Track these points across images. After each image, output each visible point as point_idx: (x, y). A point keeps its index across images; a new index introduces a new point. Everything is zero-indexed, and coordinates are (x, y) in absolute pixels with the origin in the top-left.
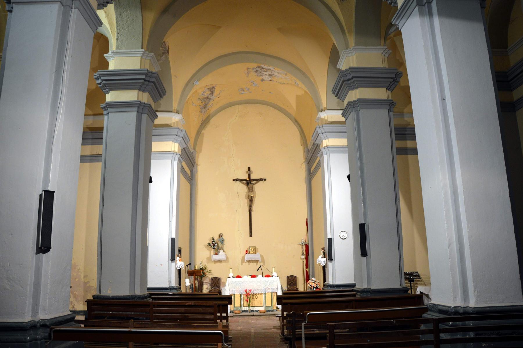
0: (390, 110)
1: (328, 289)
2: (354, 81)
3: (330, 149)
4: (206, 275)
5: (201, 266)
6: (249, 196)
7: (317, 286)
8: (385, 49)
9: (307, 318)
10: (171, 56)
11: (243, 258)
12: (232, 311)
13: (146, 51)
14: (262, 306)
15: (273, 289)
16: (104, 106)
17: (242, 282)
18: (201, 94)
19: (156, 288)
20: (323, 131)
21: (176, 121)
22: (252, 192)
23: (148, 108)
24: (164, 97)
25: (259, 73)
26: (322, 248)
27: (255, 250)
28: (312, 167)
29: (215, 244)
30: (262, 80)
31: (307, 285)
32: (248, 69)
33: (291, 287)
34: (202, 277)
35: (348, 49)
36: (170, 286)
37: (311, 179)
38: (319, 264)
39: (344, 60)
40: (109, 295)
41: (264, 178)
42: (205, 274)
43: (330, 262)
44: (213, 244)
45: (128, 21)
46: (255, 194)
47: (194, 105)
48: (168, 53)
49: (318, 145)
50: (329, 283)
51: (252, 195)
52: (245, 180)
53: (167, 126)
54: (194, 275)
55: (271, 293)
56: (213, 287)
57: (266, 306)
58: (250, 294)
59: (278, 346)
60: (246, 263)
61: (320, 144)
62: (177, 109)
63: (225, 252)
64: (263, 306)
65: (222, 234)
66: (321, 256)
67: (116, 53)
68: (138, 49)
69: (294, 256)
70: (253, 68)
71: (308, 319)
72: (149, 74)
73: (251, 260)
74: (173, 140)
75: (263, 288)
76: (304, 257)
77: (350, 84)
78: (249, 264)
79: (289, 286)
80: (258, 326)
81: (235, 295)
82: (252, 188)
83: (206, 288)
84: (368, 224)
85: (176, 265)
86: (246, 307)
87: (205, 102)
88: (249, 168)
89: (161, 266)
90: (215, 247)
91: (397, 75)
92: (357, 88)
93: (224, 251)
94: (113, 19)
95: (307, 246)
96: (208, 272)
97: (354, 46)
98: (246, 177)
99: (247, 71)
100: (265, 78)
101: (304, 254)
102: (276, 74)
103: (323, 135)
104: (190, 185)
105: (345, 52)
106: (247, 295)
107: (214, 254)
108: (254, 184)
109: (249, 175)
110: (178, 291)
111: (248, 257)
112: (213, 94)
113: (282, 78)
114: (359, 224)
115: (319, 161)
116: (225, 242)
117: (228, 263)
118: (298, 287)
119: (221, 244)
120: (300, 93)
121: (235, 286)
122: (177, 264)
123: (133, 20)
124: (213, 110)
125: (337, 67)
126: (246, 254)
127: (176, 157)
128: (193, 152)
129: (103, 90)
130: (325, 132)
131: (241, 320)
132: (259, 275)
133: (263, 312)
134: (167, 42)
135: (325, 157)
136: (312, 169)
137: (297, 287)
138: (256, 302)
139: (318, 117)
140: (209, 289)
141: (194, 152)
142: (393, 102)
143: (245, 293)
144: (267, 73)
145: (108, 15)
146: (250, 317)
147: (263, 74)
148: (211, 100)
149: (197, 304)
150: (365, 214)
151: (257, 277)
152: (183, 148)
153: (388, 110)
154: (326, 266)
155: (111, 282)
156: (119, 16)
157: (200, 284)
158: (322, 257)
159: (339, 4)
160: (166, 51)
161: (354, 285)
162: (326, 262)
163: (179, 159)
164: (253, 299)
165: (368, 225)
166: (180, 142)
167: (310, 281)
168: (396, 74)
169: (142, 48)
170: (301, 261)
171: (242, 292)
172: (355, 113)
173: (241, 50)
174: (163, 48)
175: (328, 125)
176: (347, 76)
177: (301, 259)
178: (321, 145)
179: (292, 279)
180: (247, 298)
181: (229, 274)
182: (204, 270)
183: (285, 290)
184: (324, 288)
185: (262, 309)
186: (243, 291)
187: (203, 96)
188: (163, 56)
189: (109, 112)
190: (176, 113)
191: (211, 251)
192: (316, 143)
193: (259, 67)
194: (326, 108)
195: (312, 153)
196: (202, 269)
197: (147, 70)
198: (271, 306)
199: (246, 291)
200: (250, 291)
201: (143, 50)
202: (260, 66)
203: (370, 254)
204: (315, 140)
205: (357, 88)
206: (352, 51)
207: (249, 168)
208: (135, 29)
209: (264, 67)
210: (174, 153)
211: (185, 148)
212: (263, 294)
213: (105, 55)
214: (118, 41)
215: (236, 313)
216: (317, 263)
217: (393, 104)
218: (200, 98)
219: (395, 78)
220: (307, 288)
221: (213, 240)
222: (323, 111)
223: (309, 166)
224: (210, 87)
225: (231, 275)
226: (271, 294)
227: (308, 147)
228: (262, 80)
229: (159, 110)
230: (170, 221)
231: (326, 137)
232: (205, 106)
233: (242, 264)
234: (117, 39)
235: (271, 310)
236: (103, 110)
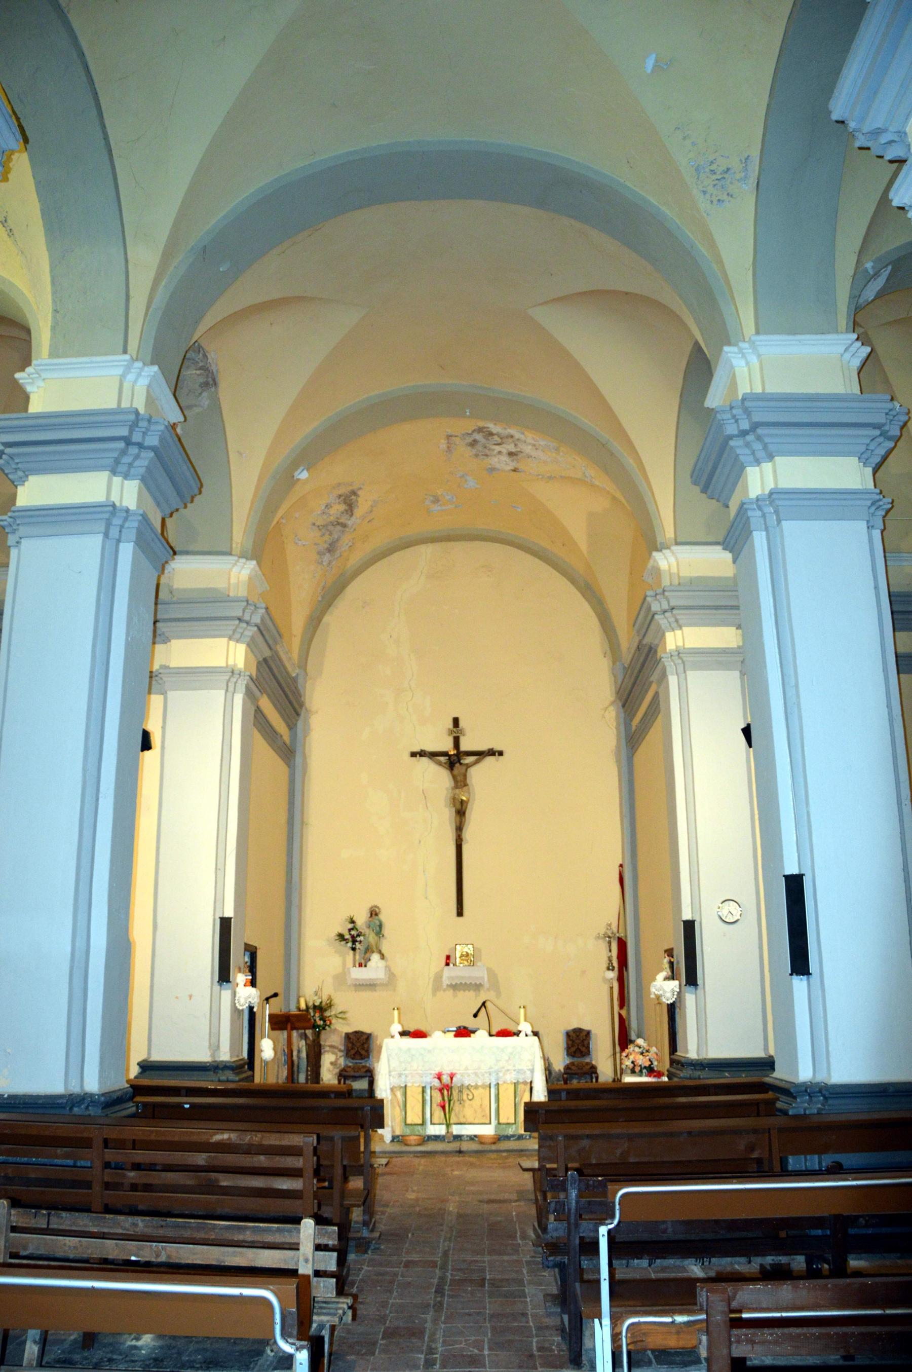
1: (685, 1073)
4: (332, 1027)
5: (316, 998)
6: (454, 799)
7: (652, 1064)
9: (617, 1207)
11: (438, 977)
12: (398, 1136)
13: (133, 360)
14: (488, 1122)
15: (519, 1071)
16: (9, 520)
17: (430, 1051)
20: (665, 606)
25: (480, 449)
29: (358, 935)
31: (621, 1060)
34: (318, 1030)
36: (217, 1059)
38: (658, 997)
42: (328, 1023)
44: (353, 937)
47: (300, 543)
51: (464, 798)
54: (289, 1027)
55: (515, 1083)
60: (444, 990)
61: (657, 645)
64: (490, 1123)
65: (378, 908)
66: (662, 975)
70: (463, 435)
71: (621, 1210)
73: (466, 983)
75: (490, 1068)
76: (612, 975)
78: (455, 996)
82: (465, 776)
83: (332, 1063)
85: (235, 997)
87: (330, 534)
88: (456, 721)
90: (358, 945)
93: (383, 957)
95: (622, 945)
98: (447, 745)
100: (499, 462)
102: (528, 449)
103: (666, 618)
104: (289, 767)
106: (441, 1090)
107: (354, 966)
108: (468, 766)
112: (352, 511)
115: (656, 695)
116: (386, 931)
117: (394, 990)
119: (376, 938)
122: (238, 995)
127: (239, 682)
128: (297, 675)
131: (421, 1168)
135: (673, 680)
138: (468, 1111)
143: (436, 1083)
144: (505, 449)
148: (347, 530)
151: (472, 1035)
152: (261, 659)
153: (865, 522)
154: (677, 1004)
155: (9, 1050)
158: (667, 979)
161: (768, 1064)
162: (679, 993)
163: (248, 688)
164: (461, 1101)
166: (252, 638)
167: (632, 1049)
168: (887, 414)
170: (605, 989)
174: (201, 368)
177: (605, 980)
178: (659, 650)
179: (579, 1039)
182: (326, 1010)
183: (560, 1070)
185: (488, 1131)
186: (432, 1076)
187: (325, 517)
195: (635, 675)
196: (319, 1009)
198: (513, 1121)
199: (439, 1078)
200: (452, 1078)
201: (127, 357)
202: (484, 428)
207: (456, 721)
213: (18, 375)
216: (652, 996)
218: (318, 523)
220: (622, 1070)
221: (351, 926)
223: (625, 712)
224: (343, 490)
225: (396, 1028)
226: (513, 1086)
228: (492, 470)
230: (219, 870)
232: (330, 545)
233: (434, 994)
235: (513, 1136)
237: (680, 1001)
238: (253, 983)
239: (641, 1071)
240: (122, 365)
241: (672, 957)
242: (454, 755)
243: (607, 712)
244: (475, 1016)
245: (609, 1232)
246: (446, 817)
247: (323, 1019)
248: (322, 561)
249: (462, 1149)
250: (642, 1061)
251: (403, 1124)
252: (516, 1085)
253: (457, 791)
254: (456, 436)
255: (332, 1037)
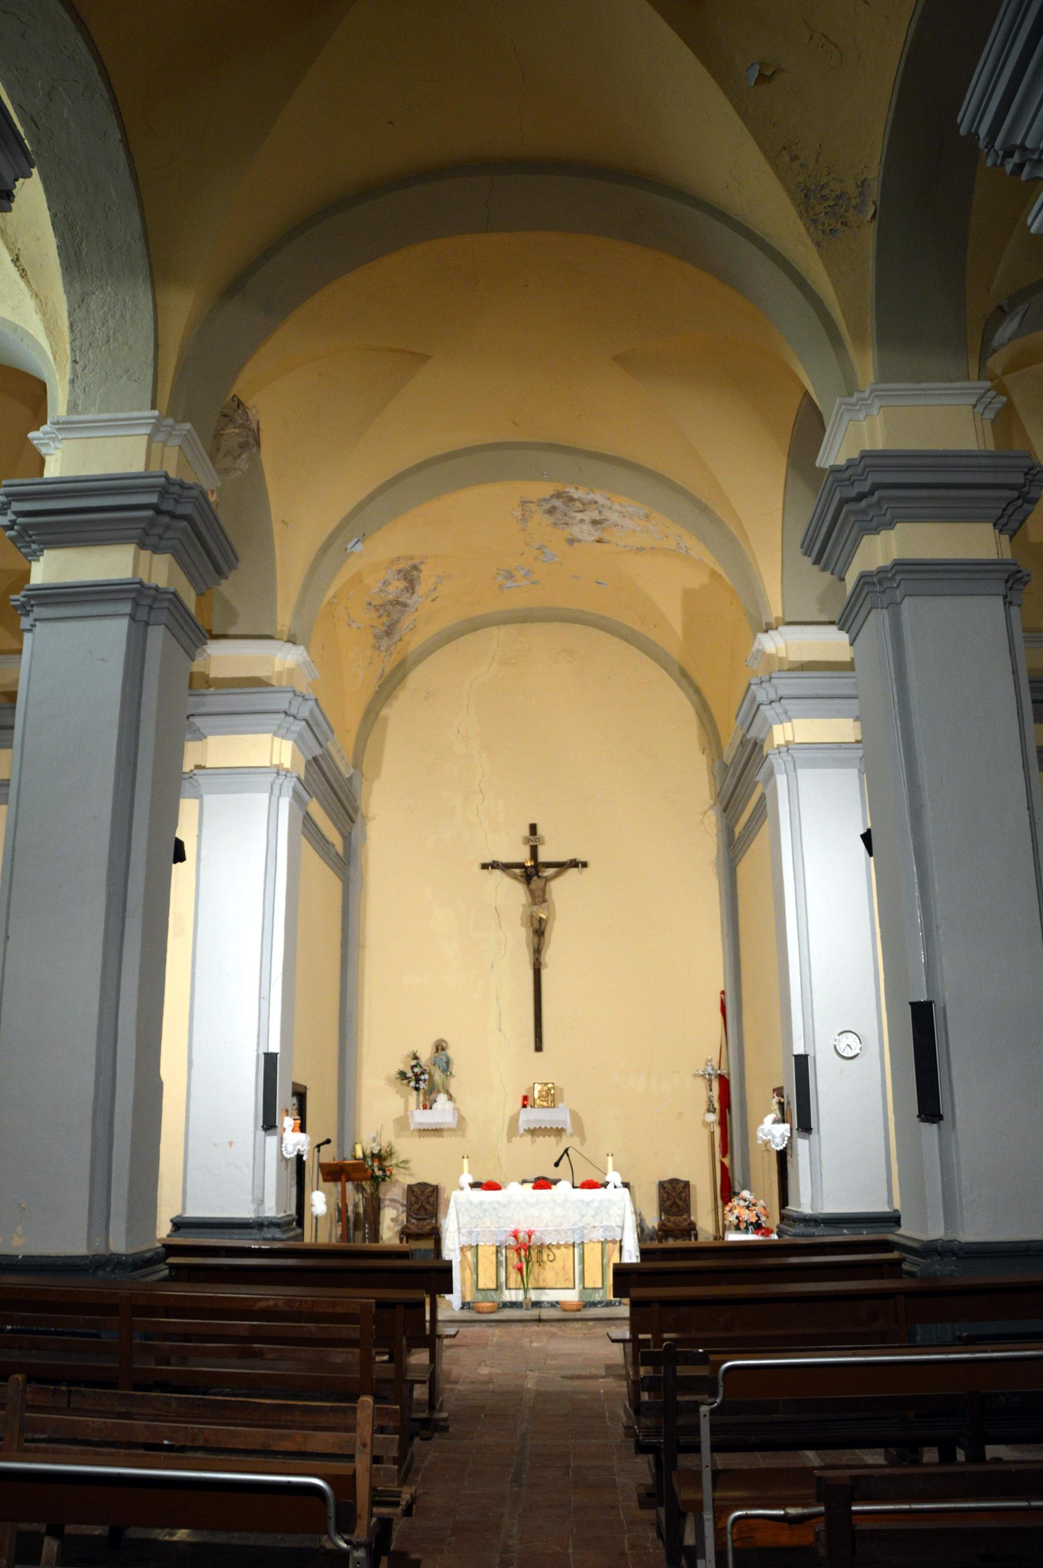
0: (1008, 599)
2: (881, 499)
3: (797, 754)
4: (393, 1178)
5: (374, 1145)
6: (532, 916)
7: (759, 1219)
8: (983, 391)
9: (721, 1383)
10: (267, 456)
11: (514, 1120)
12: (469, 1303)
14: (572, 1286)
15: (607, 1228)
16: (22, 599)
17: (504, 1206)
18: (376, 590)
19: (211, 1221)
21: (288, 669)
22: (543, 905)
23: (166, 604)
24: (232, 575)
25: (560, 517)
26: (774, 1090)
27: (551, 1097)
28: (737, 821)
29: (422, 1073)
30: (572, 541)
31: (724, 1215)
32: (524, 503)
33: (672, 1219)
34: (376, 1181)
35: (856, 395)
36: (261, 1215)
37: (737, 861)
38: (767, 1143)
39: (838, 441)
40: (16, 1254)
41: (583, 859)
42: (388, 1173)
43: (804, 1138)
44: (416, 1075)
45: (107, 321)
46: (551, 912)
48: (258, 444)
49: (756, 744)
50: (799, 1210)
51: (544, 916)
52: (520, 866)
53: (256, 683)
55: (602, 1242)
56: (415, 1216)
57: (584, 1288)
58: (529, 1247)
59: (615, 1457)
60: (521, 1136)
61: (763, 740)
62: (289, 630)
63: (455, 1102)
64: (574, 1288)
66: (771, 1117)
67: (65, 426)
68: (140, 409)
69: (681, 1114)
71: (725, 1386)
72: (172, 489)
73: (540, 1128)
74: (275, 728)
76: (713, 1118)
77: (864, 512)
78: (533, 1142)
79: (665, 1213)
80: (553, 1362)
81: (480, 1248)
82: (544, 890)
83: (392, 1220)
84: (942, 1005)
86: (516, 1289)
87: (389, 615)
88: (533, 828)
89: (231, 1146)
90: (422, 1085)
91: (1030, 477)
92: (890, 525)
93: (450, 1098)
94: (61, 317)
95: (724, 1082)
96: (397, 1166)
97: (876, 383)
98: (523, 856)
99: (521, 508)
100: (582, 532)
101: (715, 1109)
102: (614, 517)
103: (773, 709)
105: (843, 407)
106: (518, 1251)
107: (418, 1108)
108: (547, 880)
109: (534, 852)
110: (284, 1232)
111: (530, 1117)
113: (634, 531)
114: (911, 1004)
115: (763, 797)
116: (455, 1069)
117: (464, 1136)
118: (696, 1216)
119: (443, 1076)
120: (697, 579)
121: (480, 1218)
123: (123, 317)
124: (415, 642)
125: (817, 464)
126: (524, 1106)
127: (286, 784)
129: (22, 550)
130: (781, 698)
131: (495, 1339)
132: (565, 1180)
133: (575, 1308)
134: (255, 407)
135: (781, 780)
136: (738, 829)
137: (692, 1218)
138: (549, 1273)
139: (754, 649)
140: (402, 1221)
141: (354, 778)
142: (1019, 572)
143: (512, 1241)
145: (44, 304)
146: (530, 1324)
147: (574, 518)
148: (408, 610)
149: (297, 1305)
150: (930, 967)
151: (553, 1187)
152: (310, 758)
154: (789, 1151)
155: (23, 1205)
156: (79, 307)
157: (373, 1207)
158: (775, 1122)
159: (818, 245)
160: (252, 441)
161: (893, 1220)
162: (790, 1138)
164: (540, 1262)
165: (944, 1009)
166: (300, 734)
168: (1026, 474)
169: (153, 407)
170: (706, 1132)
171: (503, 1238)
172: (885, 611)
173: (498, 439)
175: (787, 674)
176: (854, 481)
177: (707, 1125)
179: (676, 1192)
180: (521, 1261)
181: (459, 1177)
182: (385, 1159)
183: (653, 1227)
184: (784, 1227)
185: (571, 1296)
186: (507, 1234)
187: (383, 596)
188: (240, 454)
189: (36, 620)
190: (288, 641)
191: (410, 1097)
192: (749, 736)
193: (559, 495)
194: (783, 618)
197: (166, 476)
198: (600, 1286)
200: (530, 1237)
201: (156, 413)
203: (953, 1114)
204: (746, 726)
205: (890, 525)
206: (869, 402)
207: (533, 828)
208: (130, 347)
209: (576, 494)
210: (278, 773)
211: (320, 759)
212: (574, 1247)
213: (31, 435)
214: (73, 387)
215: (481, 1310)
216: (760, 1142)
217: (1022, 578)
218: (374, 603)
219: (1024, 486)
220: (724, 1226)
221: (414, 1062)
222: (772, 629)
223: (727, 818)
224: (404, 565)
225: (466, 1179)
226: (600, 1245)
227: (725, 758)
228: (572, 541)
229: (231, 631)
230: (263, 998)
231: (784, 716)
232: (389, 627)
233: (509, 1140)
234: (72, 382)
235: (600, 1302)
236: (21, 615)
237: (791, 1148)
238: (303, 1128)
239: (747, 1228)
240: (152, 423)
241: (783, 1097)
242: (531, 866)
243: (706, 816)
244: (557, 1165)
245: (712, 1412)
246: (520, 937)
247: (382, 1168)
248: (380, 646)
249: (542, 1318)
250: (748, 1216)
251: (474, 1289)
252: (603, 1243)
253: (535, 908)
254: (532, 502)
255: (393, 1189)
